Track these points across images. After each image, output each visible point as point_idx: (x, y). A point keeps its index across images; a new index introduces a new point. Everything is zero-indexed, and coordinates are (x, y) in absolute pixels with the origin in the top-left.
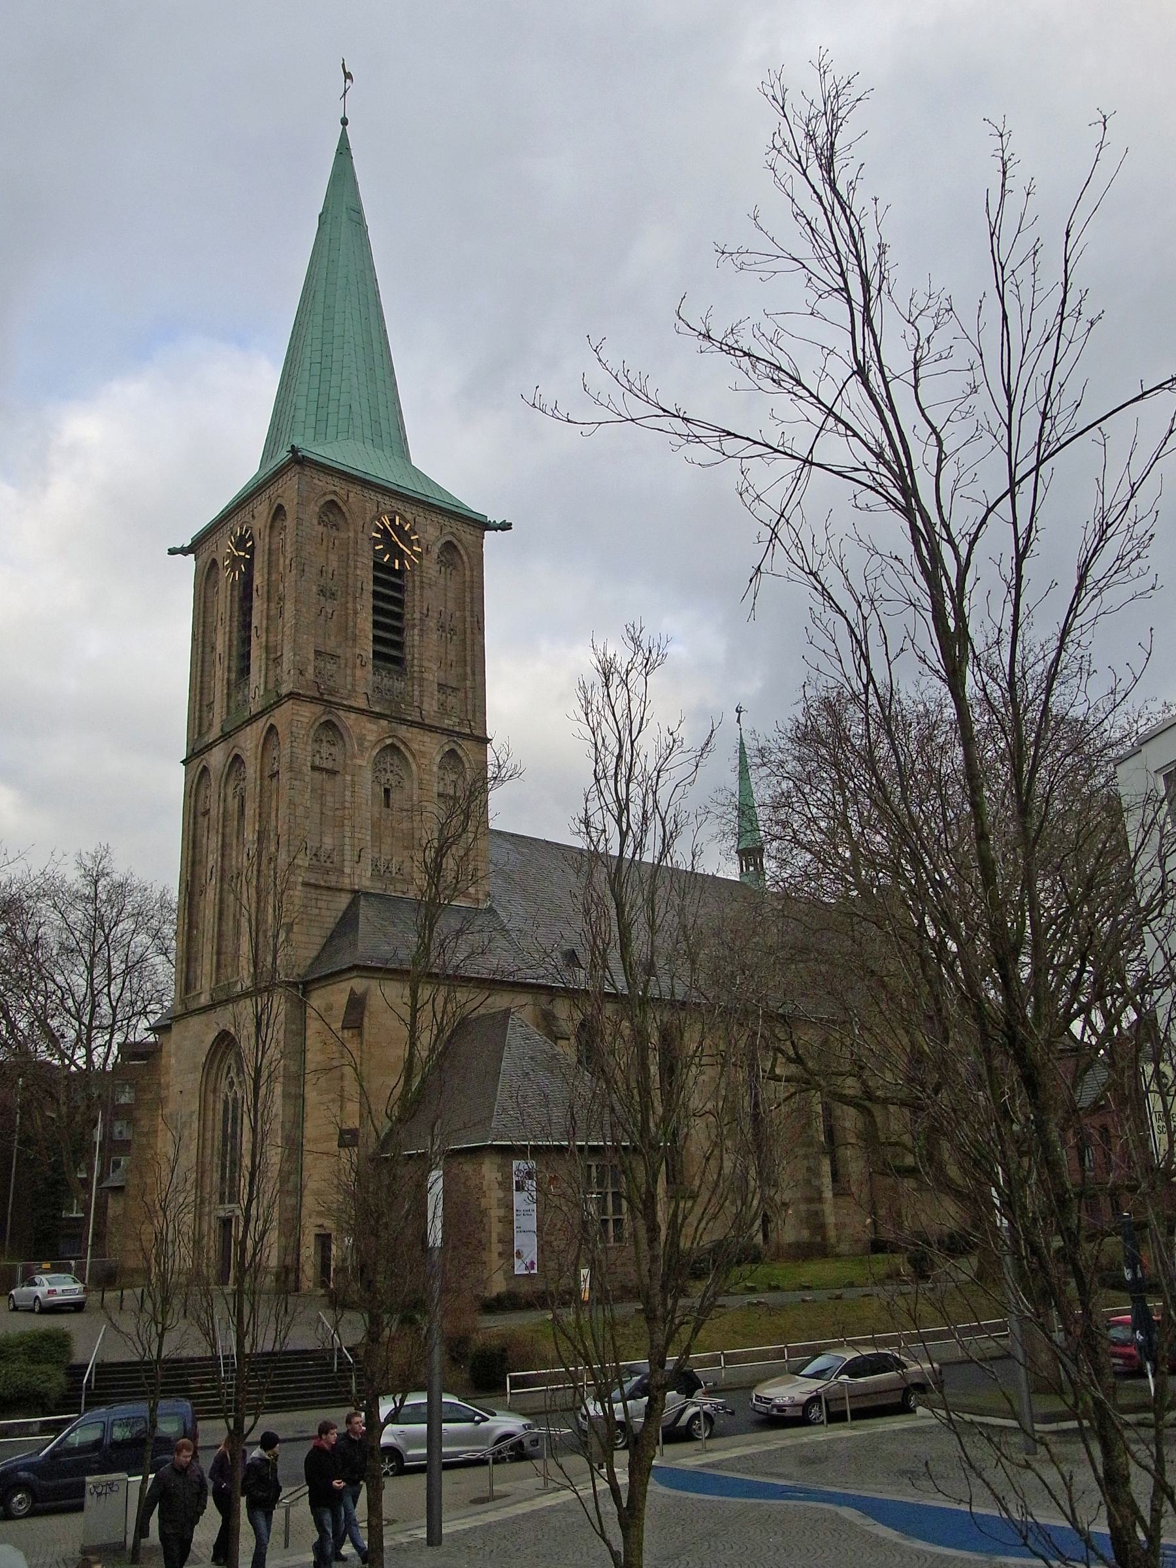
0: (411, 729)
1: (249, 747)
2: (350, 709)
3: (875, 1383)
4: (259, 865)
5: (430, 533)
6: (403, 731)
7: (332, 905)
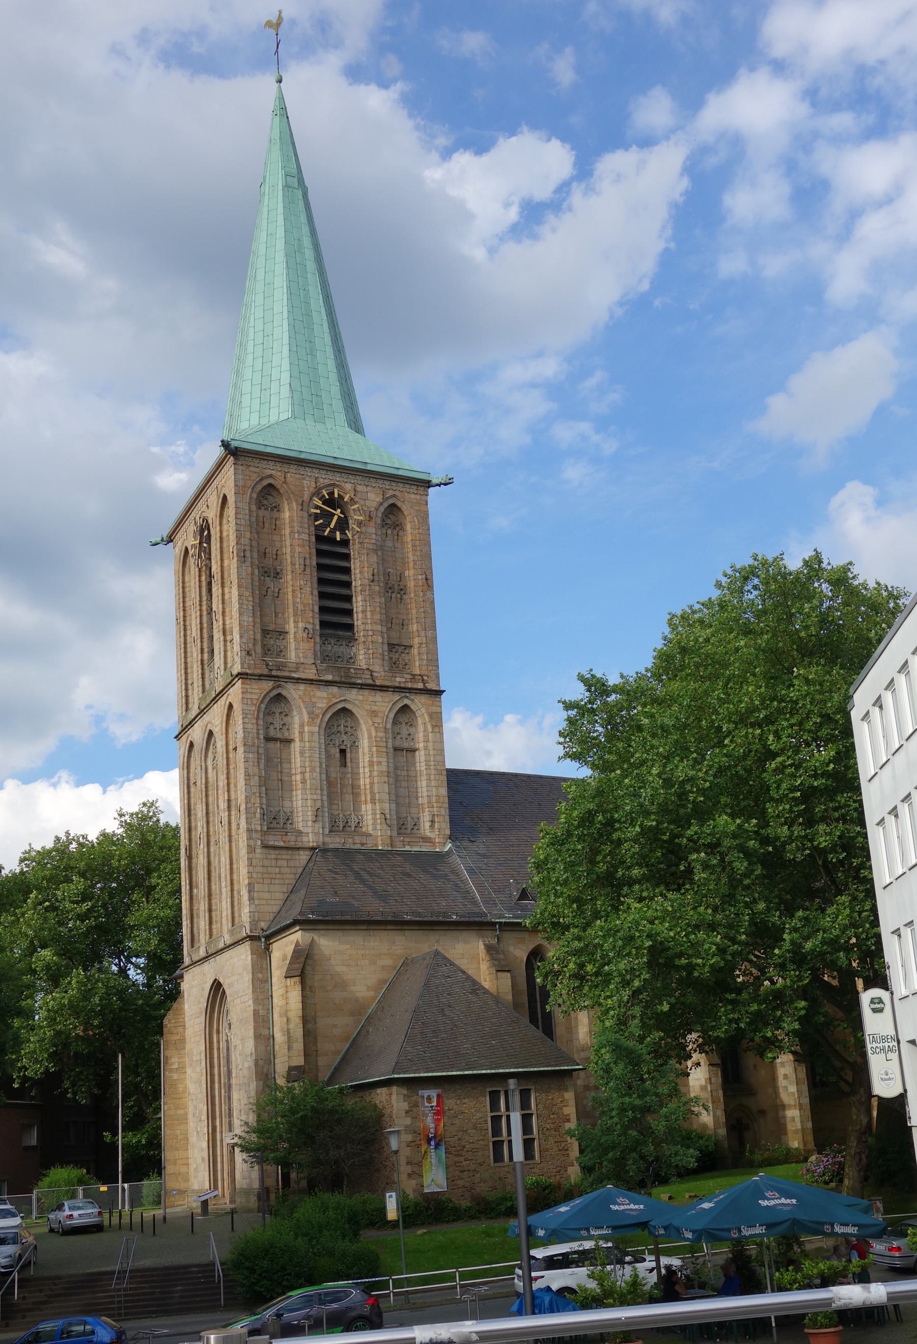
0: (361, 692)
1: (217, 723)
2: (299, 680)
3: (630, 1321)
4: (230, 830)
5: (372, 497)
6: (353, 695)
7: (292, 863)
